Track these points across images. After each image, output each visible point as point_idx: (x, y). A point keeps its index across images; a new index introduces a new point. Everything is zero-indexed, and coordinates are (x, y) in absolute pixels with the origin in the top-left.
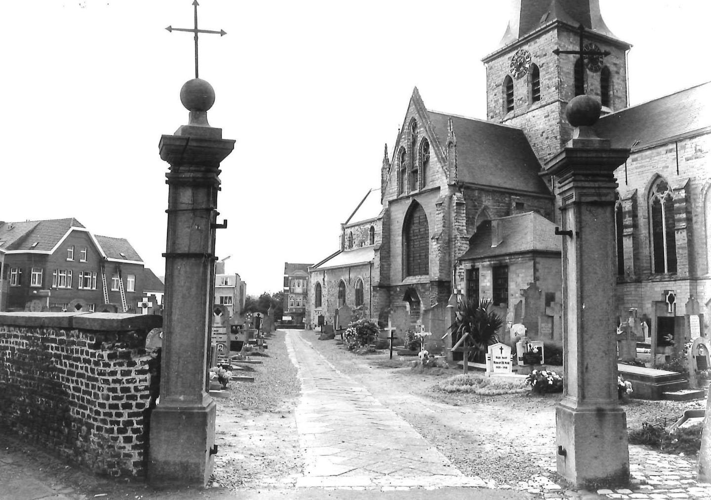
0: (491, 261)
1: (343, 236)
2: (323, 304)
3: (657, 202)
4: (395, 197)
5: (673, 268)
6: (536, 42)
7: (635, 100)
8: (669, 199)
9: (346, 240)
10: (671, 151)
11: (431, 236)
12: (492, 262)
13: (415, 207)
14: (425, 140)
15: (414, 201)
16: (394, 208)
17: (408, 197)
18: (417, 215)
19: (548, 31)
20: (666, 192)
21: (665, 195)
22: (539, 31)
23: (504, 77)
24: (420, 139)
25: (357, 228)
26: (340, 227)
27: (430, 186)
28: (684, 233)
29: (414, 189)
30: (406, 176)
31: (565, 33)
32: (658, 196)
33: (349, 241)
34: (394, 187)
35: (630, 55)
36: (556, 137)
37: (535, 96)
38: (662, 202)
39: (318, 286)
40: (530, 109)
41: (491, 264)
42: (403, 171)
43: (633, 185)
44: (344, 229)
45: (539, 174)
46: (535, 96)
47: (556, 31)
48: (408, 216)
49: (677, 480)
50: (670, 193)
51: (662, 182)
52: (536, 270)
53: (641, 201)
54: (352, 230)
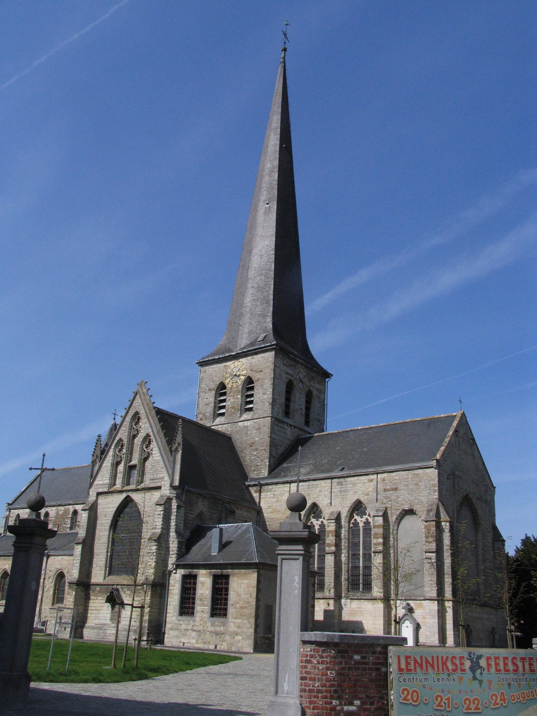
3: (356, 524)
4: (106, 490)
5: (368, 587)
6: (253, 358)
8: (367, 523)
10: (371, 481)
13: (127, 502)
14: (148, 435)
15: (128, 497)
16: (102, 501)
17: (121, 492)
19: (266, 351)
20: (365, 517)
21: (364, 520)
22: (258, 349)
23: (218, 383)
26: (5, 506)
27: (147, 483)
28: (381, 556)
29: (128, 484)
31: (281, 356)
35: (331, 384)
36: (265, 450)
38: (361, 525)
41: (211, 572)
42: (118, 463)
43: (336, 508)
45: (247, 483)
47: (273, 353)
49: (517, 696)
50: (369, 518)
53: (344, 522)
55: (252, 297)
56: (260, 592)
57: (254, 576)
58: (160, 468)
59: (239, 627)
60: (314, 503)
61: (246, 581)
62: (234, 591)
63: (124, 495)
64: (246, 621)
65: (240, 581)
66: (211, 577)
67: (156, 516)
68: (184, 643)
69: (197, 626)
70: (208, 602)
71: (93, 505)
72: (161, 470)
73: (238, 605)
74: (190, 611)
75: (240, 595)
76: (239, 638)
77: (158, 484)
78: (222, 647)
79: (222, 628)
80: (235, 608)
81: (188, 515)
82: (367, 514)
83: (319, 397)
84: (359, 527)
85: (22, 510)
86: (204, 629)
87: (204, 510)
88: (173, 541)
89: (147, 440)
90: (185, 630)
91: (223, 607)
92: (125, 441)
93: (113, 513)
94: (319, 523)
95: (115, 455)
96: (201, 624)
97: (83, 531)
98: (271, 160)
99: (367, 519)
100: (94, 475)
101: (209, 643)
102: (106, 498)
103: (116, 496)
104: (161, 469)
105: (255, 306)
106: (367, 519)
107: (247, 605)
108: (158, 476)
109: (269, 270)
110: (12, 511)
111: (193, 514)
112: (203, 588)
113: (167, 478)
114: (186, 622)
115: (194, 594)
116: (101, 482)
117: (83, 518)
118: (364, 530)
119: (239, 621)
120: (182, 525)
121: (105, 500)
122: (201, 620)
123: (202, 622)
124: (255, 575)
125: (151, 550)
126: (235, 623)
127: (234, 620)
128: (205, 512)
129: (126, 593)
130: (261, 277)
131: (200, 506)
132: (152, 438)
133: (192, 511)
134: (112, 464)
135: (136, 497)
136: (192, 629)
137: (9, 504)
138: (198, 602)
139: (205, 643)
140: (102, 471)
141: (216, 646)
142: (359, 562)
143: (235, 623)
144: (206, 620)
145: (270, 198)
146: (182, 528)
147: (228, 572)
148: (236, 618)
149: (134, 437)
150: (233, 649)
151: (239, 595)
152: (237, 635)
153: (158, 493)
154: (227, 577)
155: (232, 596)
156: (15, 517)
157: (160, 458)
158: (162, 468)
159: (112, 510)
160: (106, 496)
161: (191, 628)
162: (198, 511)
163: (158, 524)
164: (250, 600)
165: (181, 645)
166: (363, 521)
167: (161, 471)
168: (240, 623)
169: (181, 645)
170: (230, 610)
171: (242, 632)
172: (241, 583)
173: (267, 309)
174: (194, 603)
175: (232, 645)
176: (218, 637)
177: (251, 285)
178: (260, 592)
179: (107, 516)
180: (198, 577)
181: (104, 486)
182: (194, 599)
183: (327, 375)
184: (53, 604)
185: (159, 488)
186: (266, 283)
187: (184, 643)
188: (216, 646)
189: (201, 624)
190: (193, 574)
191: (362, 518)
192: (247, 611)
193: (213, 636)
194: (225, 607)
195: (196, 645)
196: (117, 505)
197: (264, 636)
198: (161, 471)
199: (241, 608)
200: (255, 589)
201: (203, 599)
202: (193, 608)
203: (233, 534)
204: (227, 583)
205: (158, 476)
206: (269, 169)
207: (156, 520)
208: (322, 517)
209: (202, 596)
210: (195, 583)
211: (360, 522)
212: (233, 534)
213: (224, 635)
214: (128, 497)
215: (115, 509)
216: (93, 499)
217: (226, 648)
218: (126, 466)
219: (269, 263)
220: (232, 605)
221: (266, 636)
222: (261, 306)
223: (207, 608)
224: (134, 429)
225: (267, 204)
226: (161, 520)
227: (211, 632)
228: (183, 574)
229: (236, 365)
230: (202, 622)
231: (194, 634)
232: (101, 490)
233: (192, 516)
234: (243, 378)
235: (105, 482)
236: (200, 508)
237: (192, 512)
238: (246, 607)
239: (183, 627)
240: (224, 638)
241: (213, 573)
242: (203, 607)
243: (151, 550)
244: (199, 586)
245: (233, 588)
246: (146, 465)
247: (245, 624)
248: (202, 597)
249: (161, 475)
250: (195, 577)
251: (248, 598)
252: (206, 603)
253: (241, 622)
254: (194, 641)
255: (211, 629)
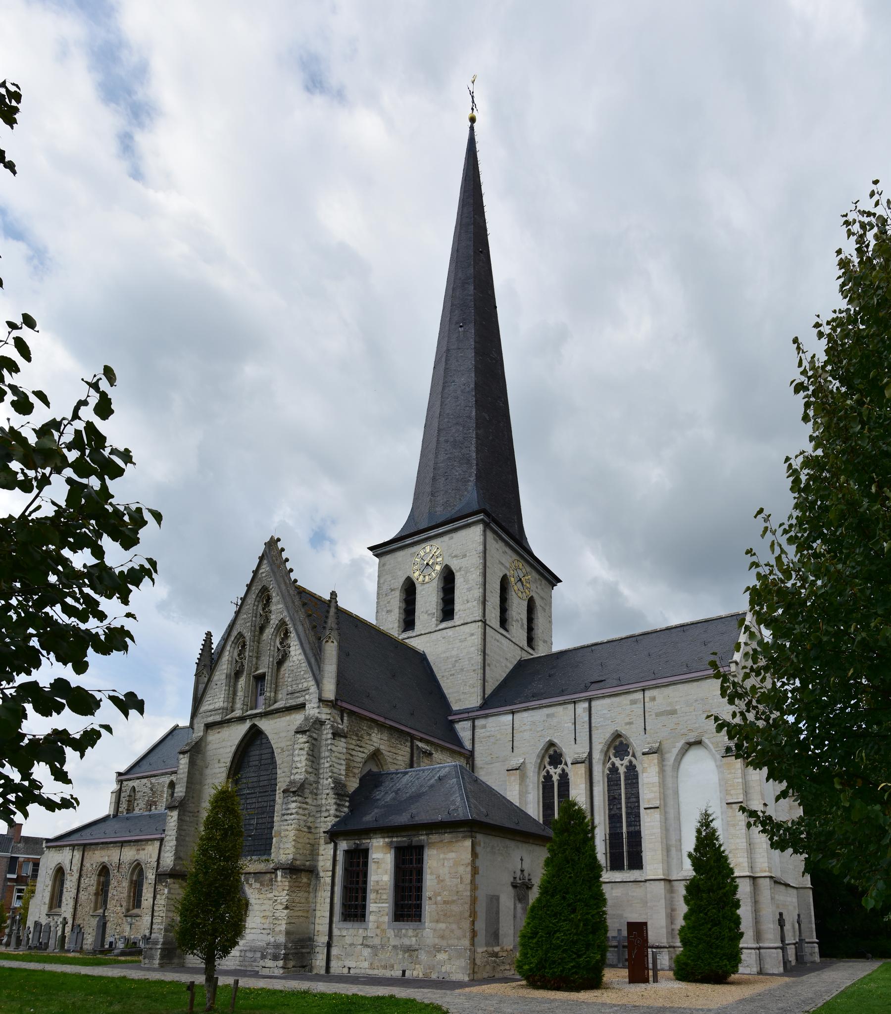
0: (392, 837)
1: (119, 793)
2: (63, 905)
4: (218, 718)
7: (559, 644)
9: (123, 800)
10: (633, 702)
11: (281, 785)
12: (395, 839)
13: (255, 736)
14: (282, 623)
15: (254, 727)
16: (214, 737)
17: (242, 719)
18: (255, 753)
21: (626, 762)
24: (274, 620)
25: (144, 781)
30: (242, 682)
32: (550, 770)
33: (129, 801)
34: (216, 700)
37: (447, 612)
39: (60, 872)
40: (437, 629)
41: (391, 842)
42: (238, 674)
44: (120, 782)
46: (447, 612)
48: (243, 744)
51: (555, 752)
52: (474, 854)
54: (135, 783)
55: (447, 454)
56: (478, 874)
57: (481, 525)
58: (302, 673)
59: (442, 937)
60: (550, 741)
61: (452, 855)
62: (431, 874)
63: (247, 724)
64: (454, 926)
65: (442, 856)
66: (393, 851)
67: (296, 752)
68: (349, 968)
69: (370, 939)
70: (388, 895)
71: (197, 743)
72: (305, 676)
73: (439, 898)
74: (359, 913)
75: (442, 881)
76: (441, 956)
77: (300, 700)
78: (415, 973)
79: (414, 939)
80: (436, 903)
81: (354, 753)
82: (631, 754)
83: (544, 610)
84: (619, 774)
85: (138, 781)
86: (383, 943)
87: (382, 747)
88: (328, 794)
89: (283, 631)
90: (351, 945)
91: (415, 902)
92: (248, 635)
93: (231, 755)
94: (559, 771)
95: (232, 661)
96: (377, 935)
97: (181, 787)
98: (463, 268)
99: (631, 762)
100: (199, 696)
101: (393, 967)
102: (219, 732)
103: (235, 728)
104: (304, 674)
105: (451, 467)
106: (631, 762)
107: (455, 898)
108: (300, 686)
109: (469, 417)
110: (125, 783)
111: (363, 752)
112: (380, 871)
113: (313, 689)
114: (348, 933)
115: (365, 882)
116: (211, 707)
117: (181, 767)
118: (626, 779)
119: (442, 926)
120: (344, 767)
121: (217, 736)
122: (378, 928)
123: (378, 932)
124: (468, 843)
125: (289, 809)
126: (435, 930)
127: (433, 925)
128: (384, 752)
129: (253, 887)
130: (458, 427)
131: (374, 739)
132: (291, 627)
133: (361, 747)
134: (228, 676)
135: (265, 725)
136: (362, 944)
137: (120, 774)
138: (371, 896)
139: (385, 967)
140: (212, 688)
141: (404, 972)
142: (621, 827)
143: (435, 930)
144: (385, 926)
145: (464, 319)
146: (343, 773)
147: (421, 840)
148: (437, 921)
149: (262, 629)
150: (434, 976)
151: (440, 880)
152: (439, 951)
153: (300, 716)
154: (419, 850)
155: (430, 882)
156: (128, 791)
157: (302, 657)
158: (306, 672)
159: (228, 750)
160: (219, 728)
161: (361, 942)
162: (372, 748)
163: (299, 765)
164: (461, 887)
165: (345, 971)
166: (624, 765)
167: (304, 678)
168: (444, 930)
169: (345, 971)
170: (427, 907)
171: (449, 946)
172: (444, 859)
173: (468, 471)
174: (364, 899)
175: (432, 968)
176: (406, 955)
177: (444, 439)
178: (478, 874)
179: (222, 760)
180: (370, 851)
181: (216, 712)
182: (364, 891)
183: (553, 580)
184: (95, 909)
185: (302, 706)
186: (466, 436)
187: (349, 968)
188: (404, 972)
189: (377, 935)
190: (363, 847)
191: (622, 760)
192: (456, 908)
193: (397, 954)
194: (418, 902)
195: (370, 972)
196: (237, 742)
197: (486, 951)
198: (304, 678)
199: (445, 902)
200: (469, 869)
201: (380, 891)
202: (364, 907)
203: (429, 780)
204: (421, 861)
205: (300, 686)
206: (460, 279)
207: (296, 759)
208: (562, 762)
209: (378, 885)
210: (366, 864)
211: (619, 766)
212: (429, 780)
213: (416, 952)
214: (254, 727)
215: (234, 748)
216: (199, 734)
217: (421, 976)
218: (250, 677)
219: (468, 408)
220: (430, 898)
221: (490, 949)
222: (459, 467)
223: (387, 905)
224: (261, 615)
225: (461, 326)
226: (303, 758)
227: (395, 947)
228: (346, 848)
229: (428, 551)
230: (378, 932)
231: (366, 952)
232: (211, 719)
233: (360, 754)
234: (438, 568)
235: (217, 706)
236: (375, 744)
237: (361, 749)
238: (453, 901)
239: (348, 940)
240: (417, 957)
241: (395, 845)
242: (380, 905)
243: (289, 809)
244: (372, 867)
245: (429, 868)
246: (282, 672)
247: (452, 931)
248: (378, 887)
249: (305, 685)
250: (365, 853)
251: (457, 885)
252: (385, 897)
253: (447, 927)
254: (366, 964)
255: (394, 942)
